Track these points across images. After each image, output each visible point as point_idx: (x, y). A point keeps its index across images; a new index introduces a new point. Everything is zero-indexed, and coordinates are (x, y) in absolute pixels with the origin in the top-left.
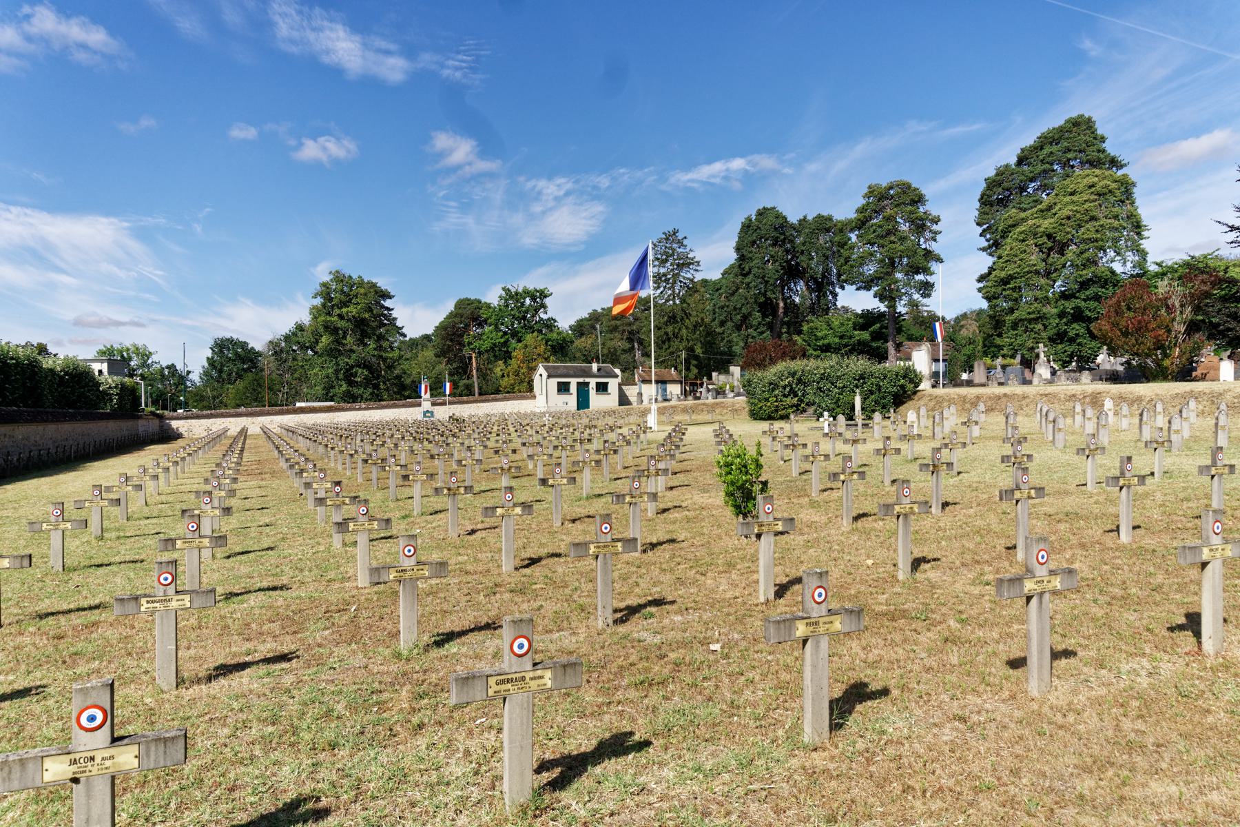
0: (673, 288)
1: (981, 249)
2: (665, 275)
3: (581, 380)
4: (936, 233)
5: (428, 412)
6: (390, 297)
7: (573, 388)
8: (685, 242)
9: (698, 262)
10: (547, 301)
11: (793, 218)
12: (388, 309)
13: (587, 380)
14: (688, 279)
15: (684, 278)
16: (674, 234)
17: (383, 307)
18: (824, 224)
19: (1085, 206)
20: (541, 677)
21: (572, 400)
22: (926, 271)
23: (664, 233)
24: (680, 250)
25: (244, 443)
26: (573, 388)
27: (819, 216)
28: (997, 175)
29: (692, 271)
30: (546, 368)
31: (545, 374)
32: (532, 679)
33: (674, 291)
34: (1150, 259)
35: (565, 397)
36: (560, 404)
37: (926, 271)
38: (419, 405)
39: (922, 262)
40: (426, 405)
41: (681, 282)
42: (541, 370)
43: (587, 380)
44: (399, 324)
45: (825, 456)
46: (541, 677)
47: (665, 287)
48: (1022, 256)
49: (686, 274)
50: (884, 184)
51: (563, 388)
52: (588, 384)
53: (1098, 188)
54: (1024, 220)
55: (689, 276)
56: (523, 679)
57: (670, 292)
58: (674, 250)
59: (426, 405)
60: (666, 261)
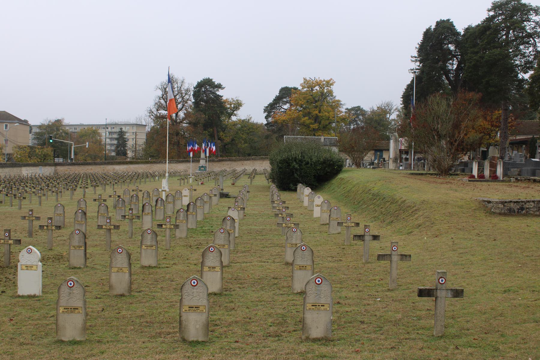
5: (202, 167)
38: (199, 161)
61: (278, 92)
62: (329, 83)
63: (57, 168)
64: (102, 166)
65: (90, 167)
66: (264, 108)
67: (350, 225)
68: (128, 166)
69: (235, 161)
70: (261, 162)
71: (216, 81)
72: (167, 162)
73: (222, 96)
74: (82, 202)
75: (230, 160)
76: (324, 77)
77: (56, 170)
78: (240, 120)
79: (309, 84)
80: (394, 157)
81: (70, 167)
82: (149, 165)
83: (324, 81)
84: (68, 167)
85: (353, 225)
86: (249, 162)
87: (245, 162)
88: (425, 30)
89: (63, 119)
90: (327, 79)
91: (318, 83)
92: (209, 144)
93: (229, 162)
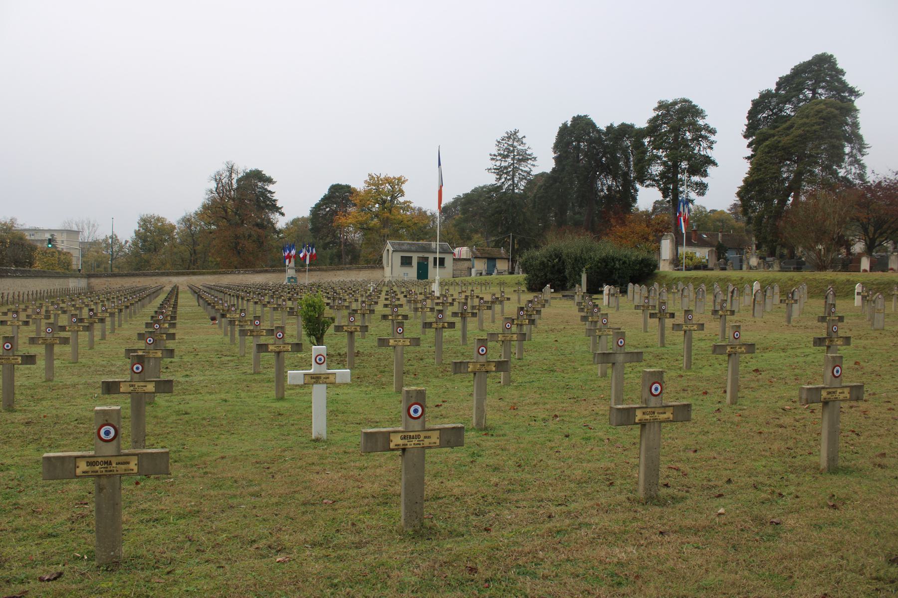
0: (513, 179)
1: (746, 158)
2: (506, 168)
3: (421, 255)
4: (712, 143)
5: (292, 278)
6: (273, 183)
7: (415, 262)
8: (524, 140)
9: (535, 158)
10: (404, 187)
11: (602, 125)
12: (270, 192)
13: (426, 255)
14: (525, 172)
15: (522, 170)
16: (515, 133)
17: (266, 190)
18: (625, 130)
19: (814, 128)
20: (17, 359)
21: (412, 273)
22: (705, 174)
23: (507, 133)
24: (519, 147)
25: (176, 301)
26: (415, 262)
27: (623, 124)
28: (761, 97)
29: (529, 166)
30: (393, 245)
31: (391, 249)
32: (13, 359)
33: (513, 181)
34: (868, 171)
35: (406, 269)
36: (402, 275)
37: (705, 174)
38: (284, 271)
39: (701, 165)
40: (291, 273)
41: (519, 174)
42: (389, 246)
43: (426, 255)
44: (279, 204)
45: (403, 316)
46: (17, 359)
47: (506, 178)
48: (765, 165)
49: (524, 167)
50: (671, 101)
51: (406, 262)
52: (427, 259)
53: (824, 113)
54: (774, 136)
55: (527, 169)
56: (9, 359)
57: (510, 182)
58: (514, 147)
59: (291, 273)
60: (507, 156)
61: (327, 190)
62: (400, 181)
63: (90, 281)
64: (154, 278)
65: (137, 279)
66: (311, 209)
67: (285, 349)
68: (190, 278)
69: (326, 270)
70: (357, 272)
71: (267, 173)
72: (684, 244)
73: (274, 193)
74: (664, 294)
75: (320, 270)
76: (393, 174)
77: (89, 284)
78: (295, 222)
79: (375, 182)
80: (671, 258)
81: (109, 279)
82: (216, 276)
83: (394, 178)
84: (106, 279)
85: (696, 329)
86: (342, 272)
87: (339, 272)
88: (757, 96)
89: (16, 220)
90: (397, 176)
91: (388, 180)
92: (310, 248)
93: (318, 273)
